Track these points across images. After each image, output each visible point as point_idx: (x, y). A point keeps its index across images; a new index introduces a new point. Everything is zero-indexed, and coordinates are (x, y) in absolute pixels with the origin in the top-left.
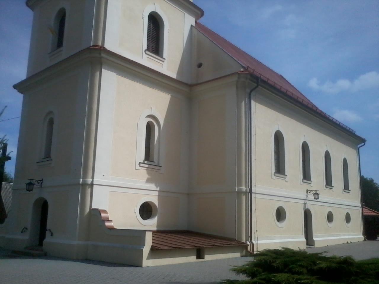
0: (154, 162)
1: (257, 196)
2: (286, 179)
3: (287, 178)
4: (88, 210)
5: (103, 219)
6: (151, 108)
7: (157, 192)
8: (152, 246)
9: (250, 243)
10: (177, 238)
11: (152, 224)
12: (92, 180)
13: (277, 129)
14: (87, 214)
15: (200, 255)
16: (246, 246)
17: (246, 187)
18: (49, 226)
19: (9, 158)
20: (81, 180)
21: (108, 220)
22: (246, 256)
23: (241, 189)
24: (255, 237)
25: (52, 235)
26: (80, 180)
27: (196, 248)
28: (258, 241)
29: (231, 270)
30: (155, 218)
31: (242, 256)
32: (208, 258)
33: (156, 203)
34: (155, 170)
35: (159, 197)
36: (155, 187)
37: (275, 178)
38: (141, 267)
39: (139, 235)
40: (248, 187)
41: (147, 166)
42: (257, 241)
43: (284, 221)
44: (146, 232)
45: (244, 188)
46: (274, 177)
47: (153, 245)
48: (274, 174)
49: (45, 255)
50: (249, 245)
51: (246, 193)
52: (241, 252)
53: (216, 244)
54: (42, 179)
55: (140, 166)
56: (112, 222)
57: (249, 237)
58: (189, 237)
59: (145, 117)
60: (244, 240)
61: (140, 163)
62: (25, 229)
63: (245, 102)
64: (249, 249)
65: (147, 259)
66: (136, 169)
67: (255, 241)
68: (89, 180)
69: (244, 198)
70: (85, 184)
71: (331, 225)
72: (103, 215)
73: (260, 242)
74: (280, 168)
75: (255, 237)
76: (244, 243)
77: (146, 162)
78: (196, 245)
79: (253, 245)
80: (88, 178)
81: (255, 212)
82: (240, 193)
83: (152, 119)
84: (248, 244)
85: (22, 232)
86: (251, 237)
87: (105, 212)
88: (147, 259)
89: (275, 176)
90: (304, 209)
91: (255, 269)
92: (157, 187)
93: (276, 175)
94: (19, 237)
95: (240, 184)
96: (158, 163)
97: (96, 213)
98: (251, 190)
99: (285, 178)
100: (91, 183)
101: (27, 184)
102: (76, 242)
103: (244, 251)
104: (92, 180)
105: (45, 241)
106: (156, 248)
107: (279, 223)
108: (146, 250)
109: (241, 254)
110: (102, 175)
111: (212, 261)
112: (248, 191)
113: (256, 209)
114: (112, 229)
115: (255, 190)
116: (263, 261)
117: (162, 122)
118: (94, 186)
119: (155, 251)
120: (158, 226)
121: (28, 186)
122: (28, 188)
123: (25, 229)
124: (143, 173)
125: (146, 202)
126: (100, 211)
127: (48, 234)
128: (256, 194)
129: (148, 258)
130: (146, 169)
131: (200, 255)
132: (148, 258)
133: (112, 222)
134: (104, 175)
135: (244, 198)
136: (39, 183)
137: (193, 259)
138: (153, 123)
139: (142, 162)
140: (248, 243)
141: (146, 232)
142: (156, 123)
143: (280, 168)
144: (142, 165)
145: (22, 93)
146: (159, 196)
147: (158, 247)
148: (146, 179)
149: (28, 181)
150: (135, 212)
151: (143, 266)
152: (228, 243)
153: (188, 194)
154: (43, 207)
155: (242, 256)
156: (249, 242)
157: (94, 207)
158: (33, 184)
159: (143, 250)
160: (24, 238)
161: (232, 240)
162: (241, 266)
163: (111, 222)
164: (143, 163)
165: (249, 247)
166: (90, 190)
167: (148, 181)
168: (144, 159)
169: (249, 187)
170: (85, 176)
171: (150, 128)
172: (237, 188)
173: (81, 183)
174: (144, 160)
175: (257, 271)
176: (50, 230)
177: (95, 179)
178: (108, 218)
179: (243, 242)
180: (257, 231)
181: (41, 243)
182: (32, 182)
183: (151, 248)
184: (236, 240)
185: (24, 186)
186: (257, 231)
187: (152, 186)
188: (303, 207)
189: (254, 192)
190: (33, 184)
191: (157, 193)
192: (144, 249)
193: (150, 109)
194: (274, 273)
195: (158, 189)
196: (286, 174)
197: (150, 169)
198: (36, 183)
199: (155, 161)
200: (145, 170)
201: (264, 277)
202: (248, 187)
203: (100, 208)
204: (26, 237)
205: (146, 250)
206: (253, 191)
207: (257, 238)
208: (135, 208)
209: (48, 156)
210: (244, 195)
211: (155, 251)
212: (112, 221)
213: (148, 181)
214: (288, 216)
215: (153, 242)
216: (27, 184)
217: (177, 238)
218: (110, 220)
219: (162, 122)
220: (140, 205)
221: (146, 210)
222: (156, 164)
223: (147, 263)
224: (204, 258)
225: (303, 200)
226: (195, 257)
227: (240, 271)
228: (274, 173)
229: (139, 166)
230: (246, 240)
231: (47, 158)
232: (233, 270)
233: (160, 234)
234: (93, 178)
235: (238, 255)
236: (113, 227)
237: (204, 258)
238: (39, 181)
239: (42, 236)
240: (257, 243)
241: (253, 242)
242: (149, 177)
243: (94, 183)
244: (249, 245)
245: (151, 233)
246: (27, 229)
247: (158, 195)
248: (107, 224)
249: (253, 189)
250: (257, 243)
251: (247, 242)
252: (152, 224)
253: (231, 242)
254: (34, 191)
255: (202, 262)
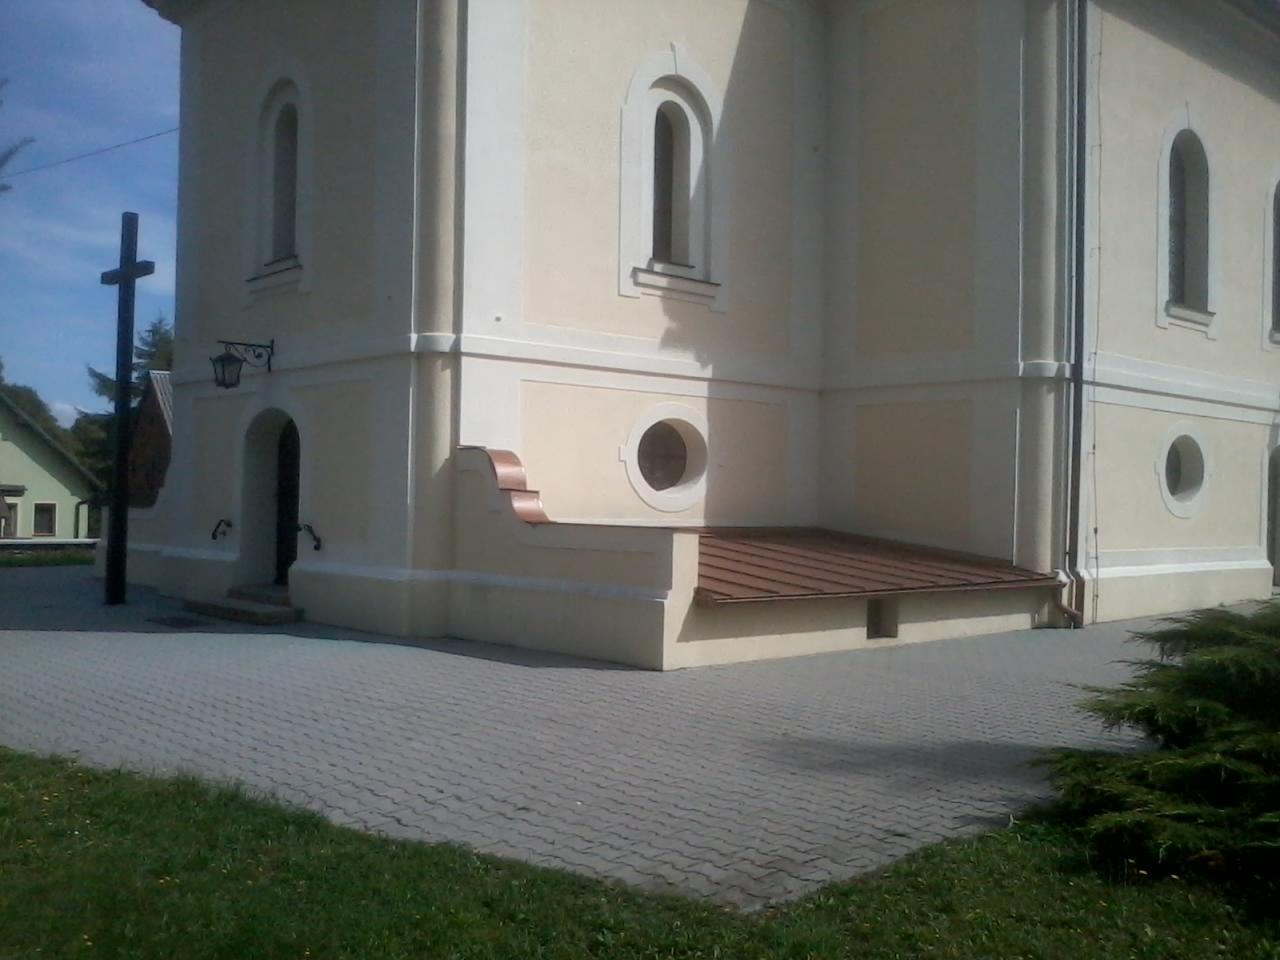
0: (693, 267)
1: (1102, 393)
2: (1212, 331)
3: (1216, 326)
4: (443, 452)
5: (502, 486)
6: (673, 47)
7: (705, 385)
8: (698, 591)
9: (1069, 577)
10: (812, 563)
11: (686, 504)
12: (454, 336)
13: (1184, 126)
14: (443, 467)
15: (880, 624)
16: (1055, 590)
17: (1058, 358)
18: (306, 512)
19: (147, 268)
20: (414, 337)
21: (521, 489)
22: (1052, 626)
23: (1039, 367)
24: (1087, 554)
25: (317, 548)
26: (409, 338)
27: (866, 596)
28: (1101, 570)
29: (1081, 707)
30: (698, 481)
31: (1037, 627)
32: (912, 633)
33: (702, 427)
34: (694, 299)
35: (712, 401)
36: (698, 365)
37: (1167, 326)
38: (661, 670)
39: (647, 547)
40: (1068, 361)
41: (663, 282)
42: (1094, 571)
43: (1198, 490)
44: (676, 537)
45: (1050, 365)
46: (1165, 321)
47: (701, 586)
48: (1167, 310)
49: (296, 621)
50: (1065, 585)
51: (1058, 381)
52: (1035, 611)
53: (943, 582)
54: (273, 342)
55: (637, 284)
56: (538, 498)
57: (1066, 553)
58: (998, 572)
59: (650, 85)
60: (1045, 566)
61: (636, 271)
62: (223, 527)
63: (1058, 7)
64: (1065, 601)
65: (679, 640)
66: (619, 295)
67: (1086, 568)
68: (444, 339)
69: (1049, 401)
70: (427, 355)
71: (1194, 505)
72: (502, 470)
73: (1105, 573)
74: (1188, 287)
75: (1087, 554)
76: (1045, 578)
77: (658, 267)
78: (868, 586)
79: (1080, 584)
80: (439, 330)
81: (1091, 456)
82: (1033, 382)
83: (676, 92)
84: (1060, 581)
85: (214, 536)
86: (1073, 555)
87: (510, 458)
88: (679, 640)
89: (1169, 315)
90: (1269, 446)
91: (1196, 704)
92: (704, 365)
93: (1175, 310)
94: (205, 552)
95: (1033, 347)
96: (707, 273)
97: (475, 464)
98: (1077, 369)
99: (1206, 325)
100: (451, 348)
101: (215, 361)
102: (406, 574)
103: (1046, 610)
104: (454, 336)
105: (295, 568)
106: (716, 597)
107: (1176, 500)
108: (677, 604)
109: (1033, 619)
110: (494, 318)
111: (926, 647)
112: (1068, 374)
113: (1094, 447)
114: (538, 523)
115: (1094, 370)
116: (1233, 670)
117: (716, 107)
118: (465, 360)
119: (713, 609)
120: (709, 512)
121: (219, 369)
122: (220, 376)
123: (223, 527)
124: (650, 312)
125: (660, 423)
126: (492, 457)
127: (303, 542)
128: (1098, 389)
129: (685, 636)
130: (659, 293)
131: (880, 624)
132: (685, 636)
133: (538, 498)
134: (498, 319)
135: (1049, 401)
136: (259, 356)
137: (852, 638)
138: (680, 109)
139: (643, 266)
140: (1063, 577)
141: (676, 537)
142: (693, 110)
143: (1188, 287)
144: (643, 278)
145: (175, 22)
146: (711, 400)
147: (721, 594)
148: (660, 333)
149: (220, 350)
150: (622, 459)
151: (666, 667)
152: (981, 576)
153: (821, 393)
154: (281, 449)
155: (1037, 627)
156: (1065, 571)
157: (465, 440)
158: (239, 361)
159: (662, 604)
160: (224, 559)
161: (1004, 565)
162: (1117, 687)
163: (534, 498)
164: (649, 271)
165: (1065, 592)
166: (447, 374)
167: (671, 340)
168: (651, 255)
169: (1073, 362)
170: (427, 321)
171: (669, 131)
172: (1021, 365)
173: (413, 347)
174: (651, 259)
175: (1204, 712)
176: (310, 529)
177: (464, 335)
178: (524, 484)
179: (1041, 572)
180: (1096, 531)
181: (281, 578)
182: (233, 351)
183: (694, 598)
184: (1014, 564)
185: (208, 371)
186: (1096, 531)
187: (685, 361)
188: (1267, 439)
189: (1090, 379)
190: (239, 361)
191: (702, 389)
192: (666, 602)
193: (670, 52)
194: (168, 431)
195: (708, 373)
196: (1210, 309)
197: (675, 295)
198: (250, 356)
199: (691, 263)
200: (658, 299)
201: (1247, 744)
202: (1068, 361)
203: (492, 444)
204: (228, 553)
205: (677, 604)
206: (1087, 375)
207: (1097, 558)
208: (623, 446)
209: (286, 252)
210: (1049, 392)
211: (713, 609)
212: (537, 492)
213: (671, 340)
214: (1211, 476)
215: (700, 576)
216: (215, 361)
217: (812, 563)
218: (529, 488)
219: (716, 107)
220: (642, 434)
221: (665, 454)
222: (697, 274)
223: (680, 653)
224: (892, 634)
225: (1266, 413)
226: (863, 631)
227: (1127, 713)
228: (1168, 302)
229: (632, 280)
230: (1054, 566)
231: (279, 261)
232: (1093, 710)
233: (720, 543)
234: (457, 328)
235: (1021, 621)
236: (542, 515)
237: (892, 634)
238: (260, 350)
239: (286, 553)
240: (1095, 576)
241: (1081, 574)
242: (674, 325)
243: (463, 349)
244: (1065, 585)
245: (694, 539)
246: (229, 524)
247: (706, 394)
248: (520, 504)
249: (1087, 366)
250: (1095, 576)
251: (1058, 573)
252: (686, 504)
253: (999, 575)
254: (243, 387)
255: (892, 649)
